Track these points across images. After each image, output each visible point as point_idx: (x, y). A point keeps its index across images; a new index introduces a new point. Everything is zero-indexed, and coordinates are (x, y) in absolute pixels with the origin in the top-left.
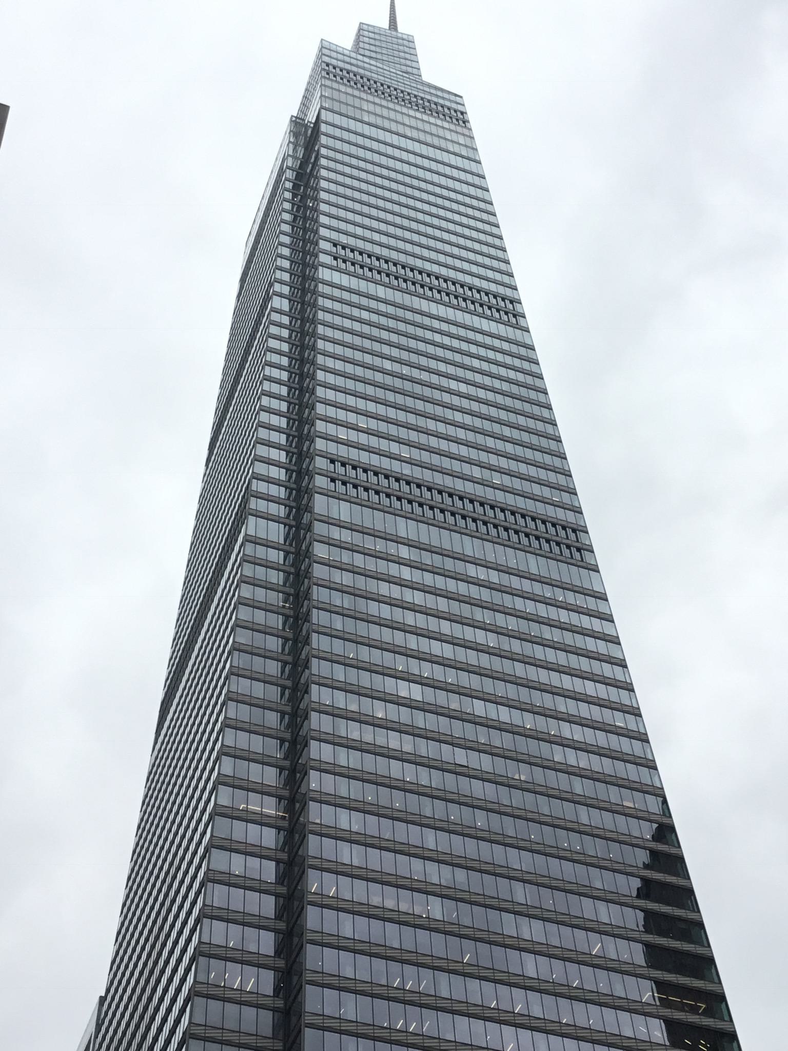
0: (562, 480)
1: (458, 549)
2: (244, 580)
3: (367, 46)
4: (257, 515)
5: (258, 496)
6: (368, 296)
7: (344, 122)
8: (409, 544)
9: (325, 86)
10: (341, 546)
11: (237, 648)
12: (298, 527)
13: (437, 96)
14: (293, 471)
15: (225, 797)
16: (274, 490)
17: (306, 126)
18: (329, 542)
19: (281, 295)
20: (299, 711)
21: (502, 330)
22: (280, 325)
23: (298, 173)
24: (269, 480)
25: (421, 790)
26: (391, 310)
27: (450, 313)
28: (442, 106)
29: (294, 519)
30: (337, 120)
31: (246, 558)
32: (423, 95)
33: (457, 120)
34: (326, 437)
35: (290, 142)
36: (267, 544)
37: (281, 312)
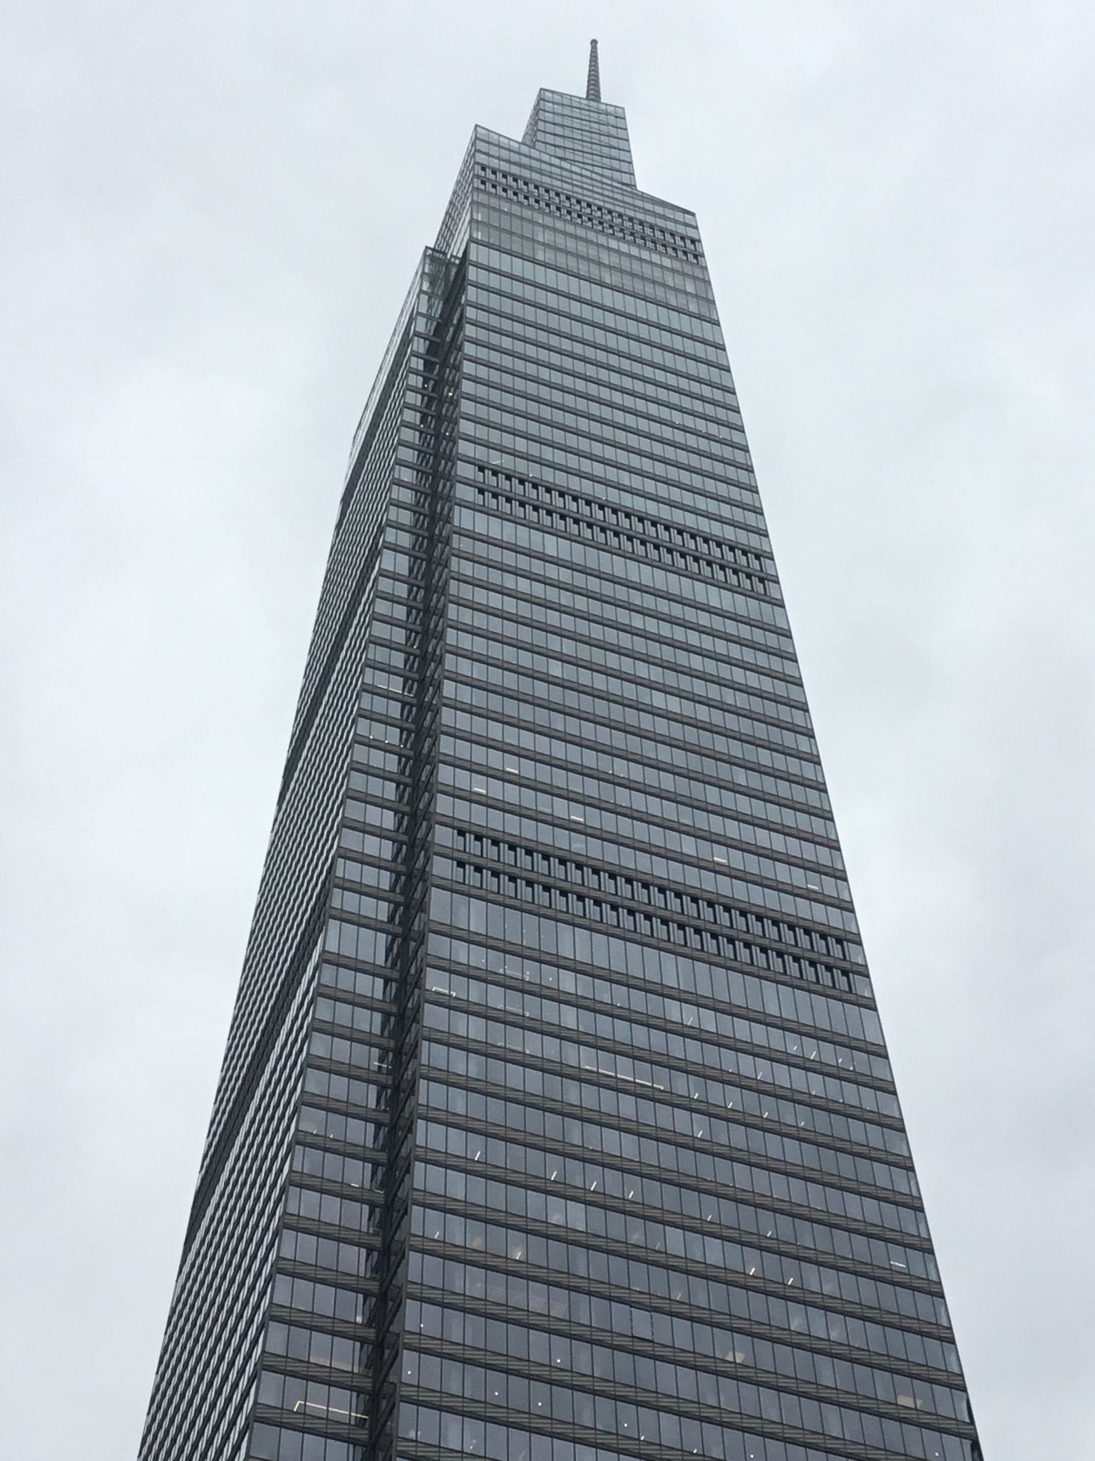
0: (823, 855)
1: (653, 976)
2: (319, 1027)
3: (550, 128)
4: (344, 917)
5: (348, 886)
6: (531, 554)
7: (505, 262)
8: (576, 968)
9: (478, 204)
10: (469, 974)
11: (301, 1140)
12: (406, 939)
13: (655, 214)
14: (404, 814)
15: (270, 1390)
16: (371, 876)
17: (448, 264)
18: (451, 968)
19: (395, 549)
20: (399, 1160)
21: (741, 605)
22: (393, 599)
23: (431, 342)
24: (363, 860)
25: (578, 1381)
26: (565, 575)
27: (659, 579)
28: (662, 231)
29: (402, 893)
30: (495, 259)
31: (322, 990)
32: (631, 214)
33: (685, 253)
34: (455, 793)
35: (421, 291)
36: (357, 967)
37: (395, 577)
